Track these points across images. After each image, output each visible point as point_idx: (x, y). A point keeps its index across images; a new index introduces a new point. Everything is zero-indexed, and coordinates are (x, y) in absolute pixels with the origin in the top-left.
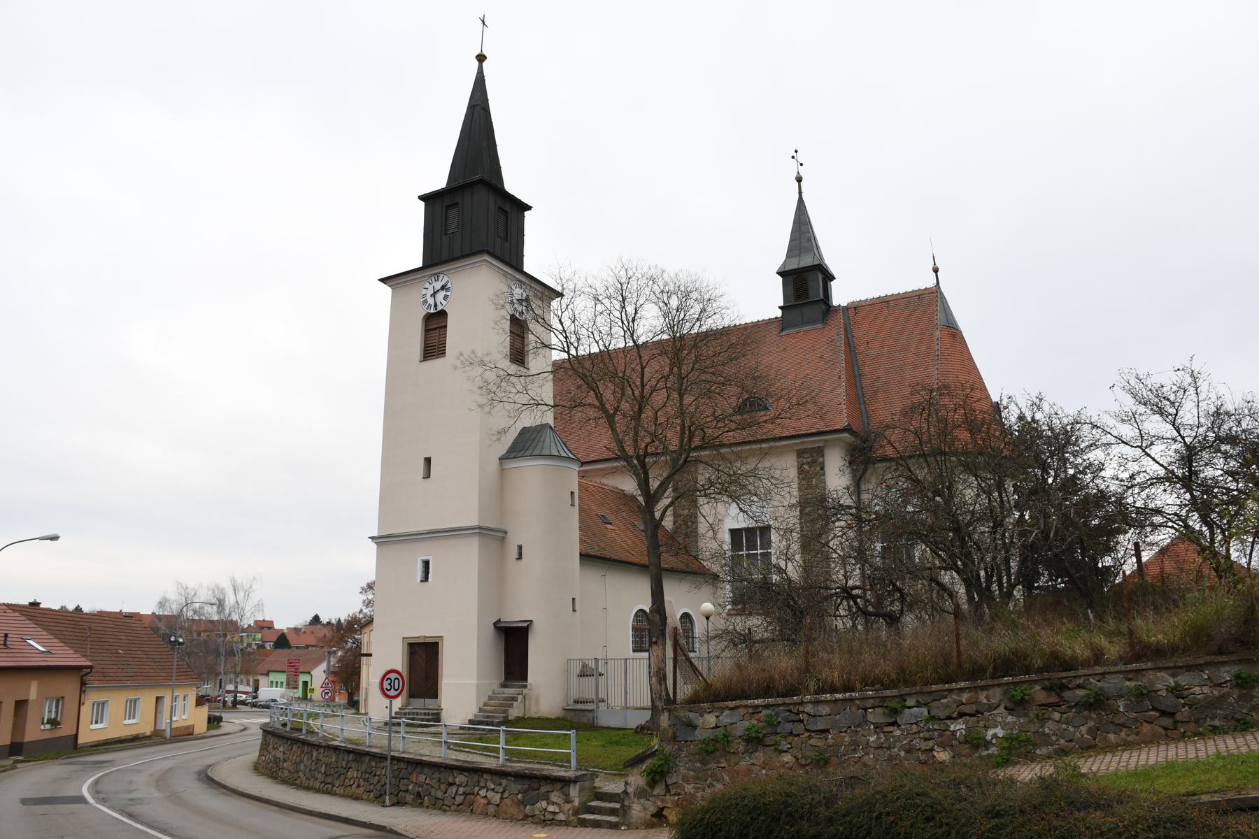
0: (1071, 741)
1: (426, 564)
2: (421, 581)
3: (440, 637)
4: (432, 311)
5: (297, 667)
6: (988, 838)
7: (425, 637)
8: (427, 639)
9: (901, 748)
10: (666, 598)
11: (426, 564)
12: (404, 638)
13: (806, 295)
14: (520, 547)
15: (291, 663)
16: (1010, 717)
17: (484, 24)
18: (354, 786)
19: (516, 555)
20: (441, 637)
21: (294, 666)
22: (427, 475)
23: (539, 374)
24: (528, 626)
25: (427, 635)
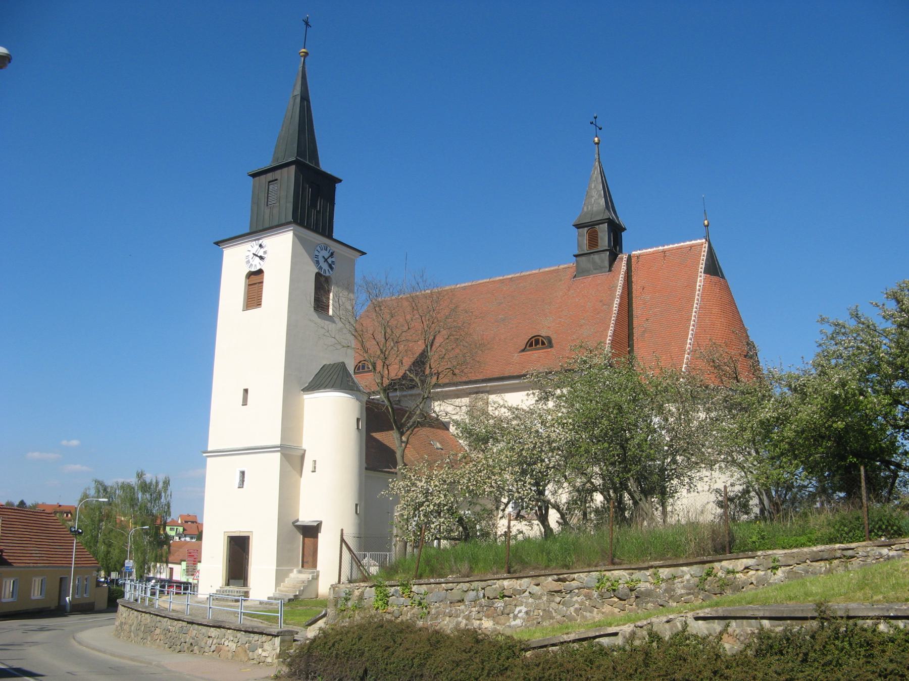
0: (564, 616)
5: (195, 557)
9: (464, 617)
12: (225, 532)
13: (596, 245)
15: (190, 553)
16: (530, 599)
18: (159, 640)
20: (252, 532)
21: (193, 556)
22: (245, 403)
25: (242, 530)
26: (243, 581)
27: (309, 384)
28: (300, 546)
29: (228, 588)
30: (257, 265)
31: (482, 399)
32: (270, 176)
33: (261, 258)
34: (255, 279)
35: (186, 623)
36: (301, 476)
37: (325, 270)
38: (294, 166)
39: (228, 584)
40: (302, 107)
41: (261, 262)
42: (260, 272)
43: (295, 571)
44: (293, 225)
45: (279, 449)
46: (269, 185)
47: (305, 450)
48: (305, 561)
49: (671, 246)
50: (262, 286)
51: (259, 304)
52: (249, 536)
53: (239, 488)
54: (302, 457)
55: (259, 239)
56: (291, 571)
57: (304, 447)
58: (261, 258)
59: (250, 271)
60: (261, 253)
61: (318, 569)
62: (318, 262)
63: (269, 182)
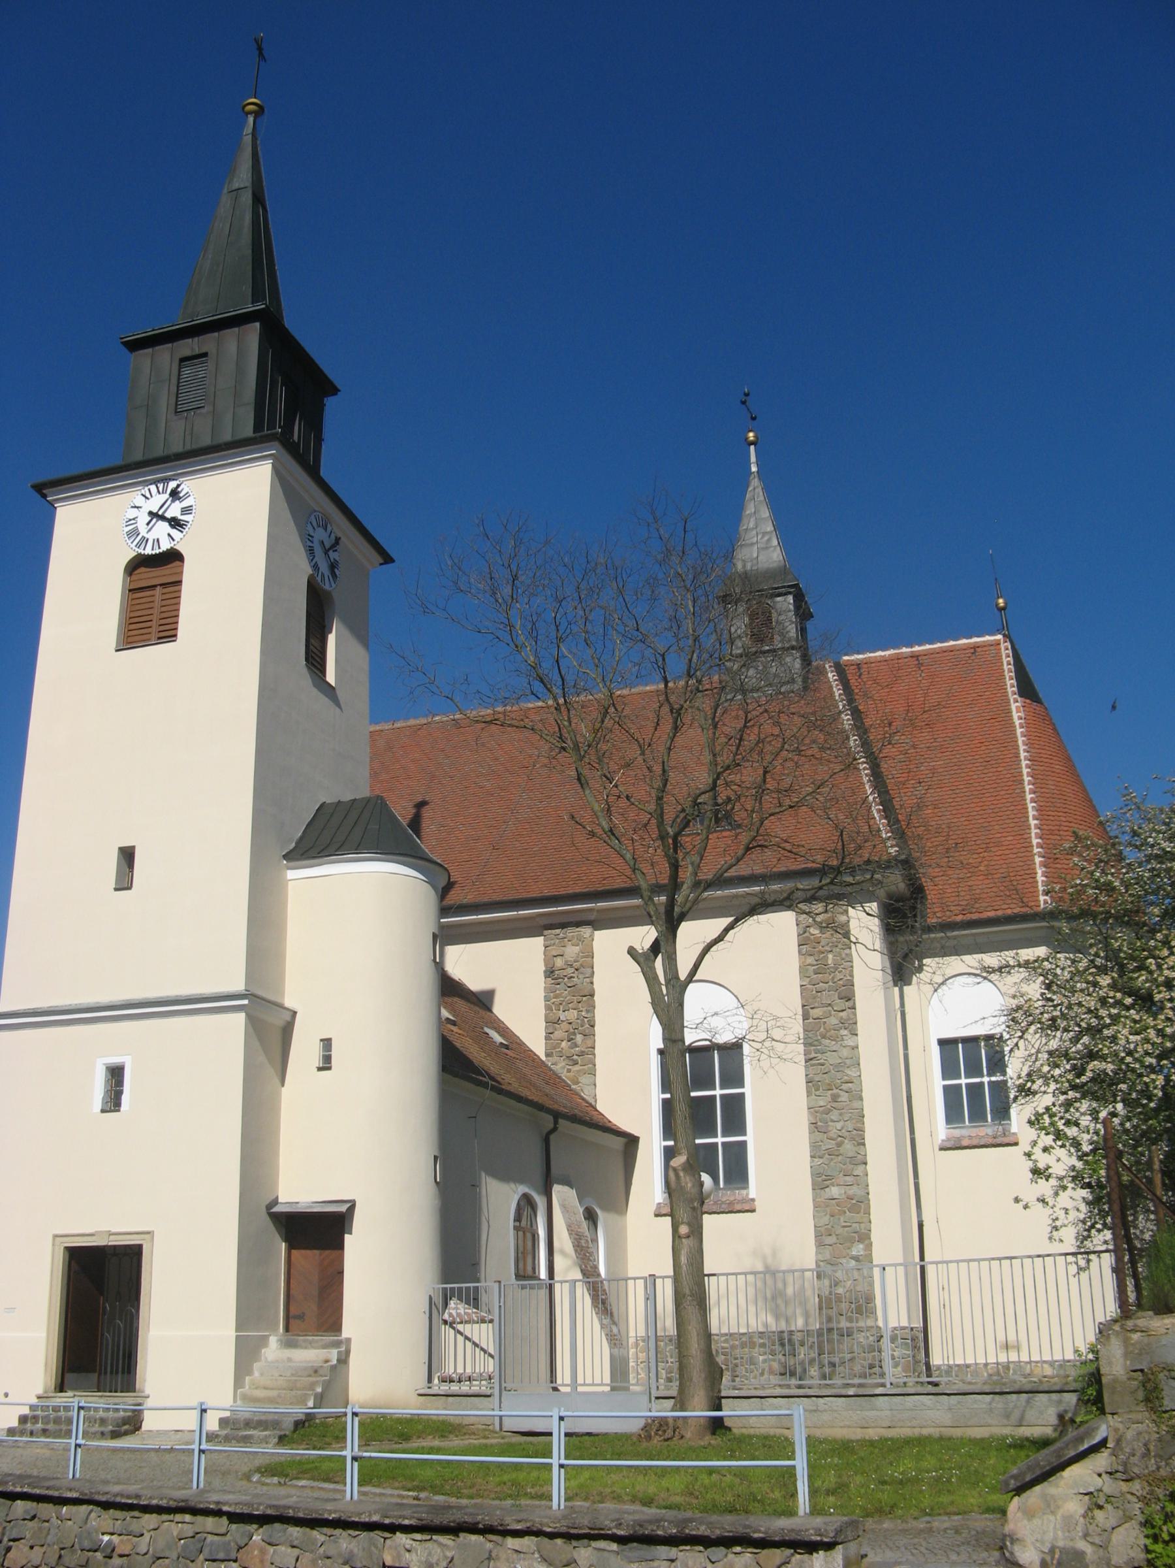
1: (116, 1074)
2: (103, 1111)
3: (148, 1233)
4: (149, 551)
6: (1086, 1567)
7: (111, 1234)
8: (112, 1238)
10: (250, 251)
11: (116, 1074)
12: (55, 1236)
14: (327, 1043)
17: (261, 55)
19: (316, 1060)
23: (441, 866)
24: (348, 1209)
25: (114, 1230)
26: (96, 1375)
27: (298, 843)
28: (278, 1274)
29: (71, 1399)
30: (161, 538)
31: (581, 939)
32: (188, 347)
33: (175, 523)
34: (147, 576)
35: (225, 1520)
36: (283, 1085)
37: (323, 575)
38: (257, 325)
39: (61, 1387)
40: (255, 214)
41: (175, 533)
42: (173, 557)
43: (273, 1341)
44: (276, 444)
45: (246, 1002)
46: (180, 368)
47: (295, 1013)
48: (291, 1314)
49: (928, 647)
50: (180, 591)
51: (168, 634)
52: (140, 1247)
53: (320, 1069)
54: (287, 1031)
55: (166, 480)
56: (264, 1341)
57: (289, 1002)
58: (175, 523)
59: (139, 555)
60: (174, 511)
61: (345, 1333)
62: (311, 551)
63: (182, 360)
